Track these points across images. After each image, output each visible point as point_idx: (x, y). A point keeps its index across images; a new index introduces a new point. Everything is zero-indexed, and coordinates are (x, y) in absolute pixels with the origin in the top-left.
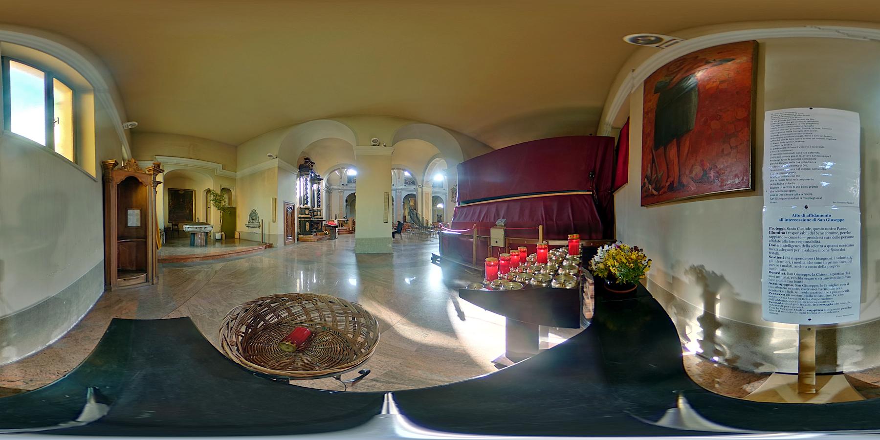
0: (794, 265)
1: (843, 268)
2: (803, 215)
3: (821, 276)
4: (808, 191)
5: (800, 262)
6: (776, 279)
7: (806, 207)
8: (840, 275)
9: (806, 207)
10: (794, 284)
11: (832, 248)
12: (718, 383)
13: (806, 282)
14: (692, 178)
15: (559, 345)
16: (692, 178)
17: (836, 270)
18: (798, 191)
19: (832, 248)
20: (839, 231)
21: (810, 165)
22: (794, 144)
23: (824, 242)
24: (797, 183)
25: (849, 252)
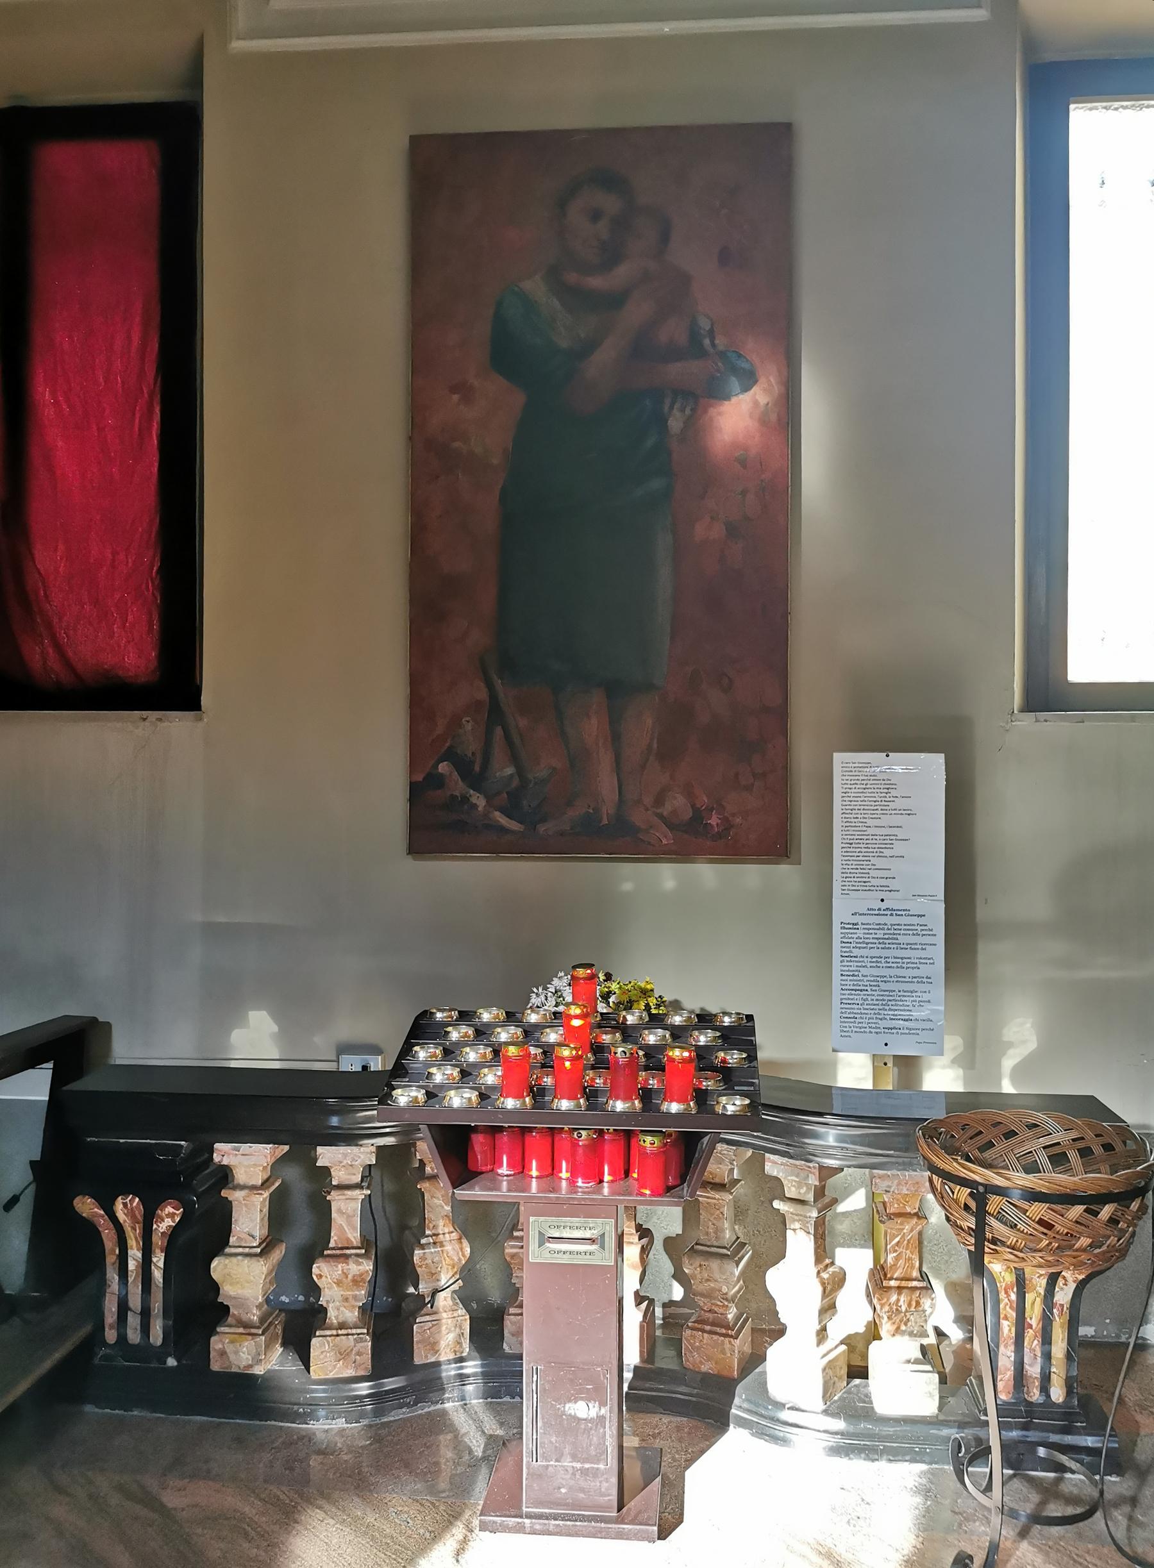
0: (869, 965)
1: (924, 970)
2: (879, 909)
3: (900, 979)
4: (884, 882)
5: (876, 961)
6: (850, 984)
7: (882, 900)
8: (920, 980)
9: (882, 900)
10: (868, 988)
11: (911, 946)
12: (898, 1300)
13: (883, 986)
14: (661, 816)
15: (74, 1080)
16: (661, 816)
17: (916, 973)
18: (874, 882)
19: (911, 946)
20: (919, 928)
21: (887, 852)
22: (870, 822)
23: (901, 939)
24: (873, 873)
25: (930, 952)
